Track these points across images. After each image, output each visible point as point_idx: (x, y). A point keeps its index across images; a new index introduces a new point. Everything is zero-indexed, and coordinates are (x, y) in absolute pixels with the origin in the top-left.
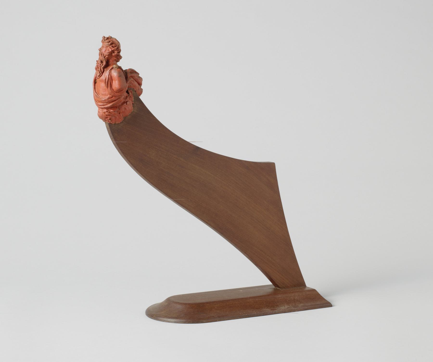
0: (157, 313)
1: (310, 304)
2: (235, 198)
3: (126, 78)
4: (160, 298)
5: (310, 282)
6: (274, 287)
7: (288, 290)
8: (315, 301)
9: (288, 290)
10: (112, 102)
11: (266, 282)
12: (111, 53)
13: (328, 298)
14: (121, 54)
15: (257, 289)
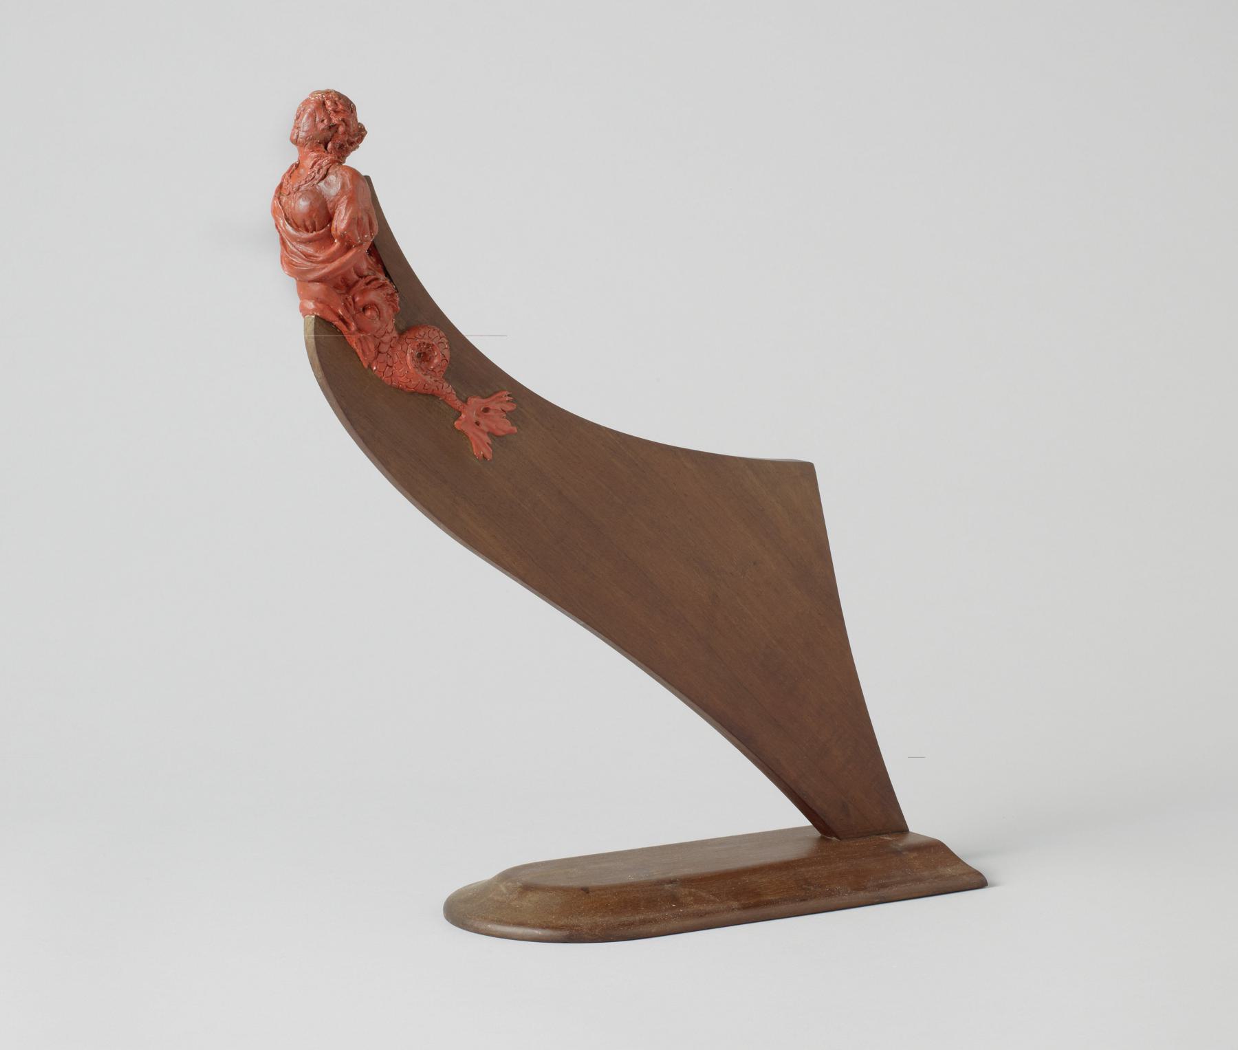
0: (471, 911)
1: (895, 889)
2: (698, 570)
3: (409, 329)
4: (482, 868)
5: (921, 819)
6: (817, 834)
7: (855, 844)
8: (938, 872)
9: (855, 844)
10: (548, 927)
11: (792, 818)
12: (334, 128)
13: (975, 864)
14: (361, 118)
15: (667, 887)
